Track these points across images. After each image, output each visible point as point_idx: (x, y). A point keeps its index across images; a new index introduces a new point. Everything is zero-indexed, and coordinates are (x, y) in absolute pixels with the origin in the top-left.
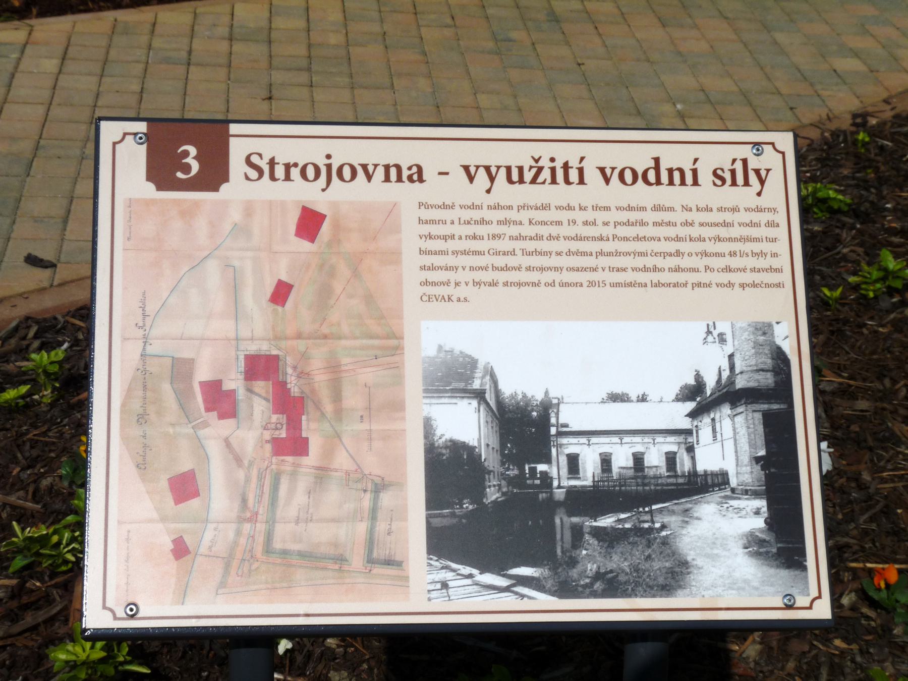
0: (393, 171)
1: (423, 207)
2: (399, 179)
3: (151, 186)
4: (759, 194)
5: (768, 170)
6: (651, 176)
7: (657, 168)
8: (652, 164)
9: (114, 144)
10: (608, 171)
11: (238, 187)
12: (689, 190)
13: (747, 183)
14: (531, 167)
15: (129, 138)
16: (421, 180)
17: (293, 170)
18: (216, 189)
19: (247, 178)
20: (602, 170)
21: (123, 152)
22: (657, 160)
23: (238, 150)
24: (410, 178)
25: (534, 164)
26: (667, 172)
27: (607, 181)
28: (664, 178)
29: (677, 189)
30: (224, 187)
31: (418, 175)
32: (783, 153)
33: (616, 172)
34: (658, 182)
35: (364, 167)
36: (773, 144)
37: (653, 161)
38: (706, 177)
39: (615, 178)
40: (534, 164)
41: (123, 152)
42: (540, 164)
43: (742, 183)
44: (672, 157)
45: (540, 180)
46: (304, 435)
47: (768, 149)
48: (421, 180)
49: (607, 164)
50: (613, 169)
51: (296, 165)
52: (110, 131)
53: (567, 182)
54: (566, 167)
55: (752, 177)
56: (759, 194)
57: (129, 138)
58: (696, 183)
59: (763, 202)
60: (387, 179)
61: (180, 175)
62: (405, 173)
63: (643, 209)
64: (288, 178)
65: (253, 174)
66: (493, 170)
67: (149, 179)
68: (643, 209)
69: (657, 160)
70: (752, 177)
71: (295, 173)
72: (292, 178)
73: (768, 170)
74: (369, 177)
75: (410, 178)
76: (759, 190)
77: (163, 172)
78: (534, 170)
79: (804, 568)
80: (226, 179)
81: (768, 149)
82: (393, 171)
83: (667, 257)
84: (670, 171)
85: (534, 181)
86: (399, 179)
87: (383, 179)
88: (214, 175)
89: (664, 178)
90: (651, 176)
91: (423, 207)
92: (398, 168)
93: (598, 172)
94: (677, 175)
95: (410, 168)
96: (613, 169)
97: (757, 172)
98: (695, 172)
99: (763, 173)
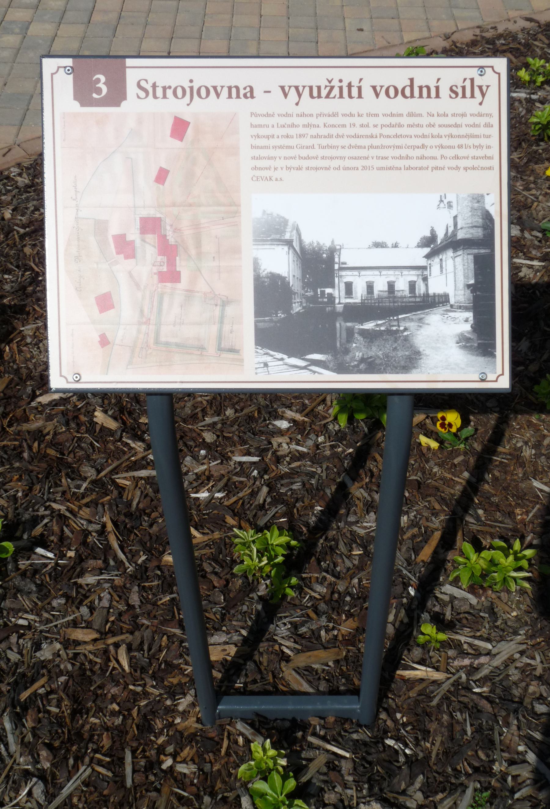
0: (234, 91)
2: (238, 97)
3: (77, 104)
4: (481, 104)
5: (488, 87)
6: (408, 92)
7: (412, 86)
8: (408, 83)
9: (52, 74)
10: (378, 89)
11: (132, 103)
12: (433, 101)
13: (473, 96)
14: (326, 86)
16: (252, 97)
17: (168, 90)
18: (118, 105)
19: (138, 97)
20: (374, 88)
22: (412, 80)
24: (245, 96)
25: (328, 84)
27: (377, 95)
29: (425, 101)
30: (124, 103)
31: (251, 94)
32: (499, 74)
34: (412, 96)
35: (215, 88)
36: (492, 67)
38: (445, 92)
39: (383, 94)
40: (328, 84)
42: (332, 84)
45: (332, 95)
47: (489, 71)
48: (252, 97)
49: (378, 84)
50: (382, 87)
51: (170, 87)
53: (350, 96)
54: (350, 86)
55: (477, 91)
56: (481, 104)
57: (61, 70)
58: (438, 96)
59: (483, 109)
60: (230, 96)
61: (95, 96)
62: (242, 92)
64: (165, 97)
65: (142, 94)
66: (301, 89)
67: (75, 98)
69: (412, 80)
71: (169, 93)
73: (488, 87)
75: (245, 96)
77: (84, 94)
78: (328, 89)
80: (125, 98)
81: (489, 71)
82: (234, 91)
84: (421, 88)
85: (327, 96)
88: (117, 96)
90: (408, 92)
92: (237, 88)
94: (425, 91)
95: (245, 89)
96: (382, 87)
97: (480, 88)
98: (437, 88)
99: (484, 89)
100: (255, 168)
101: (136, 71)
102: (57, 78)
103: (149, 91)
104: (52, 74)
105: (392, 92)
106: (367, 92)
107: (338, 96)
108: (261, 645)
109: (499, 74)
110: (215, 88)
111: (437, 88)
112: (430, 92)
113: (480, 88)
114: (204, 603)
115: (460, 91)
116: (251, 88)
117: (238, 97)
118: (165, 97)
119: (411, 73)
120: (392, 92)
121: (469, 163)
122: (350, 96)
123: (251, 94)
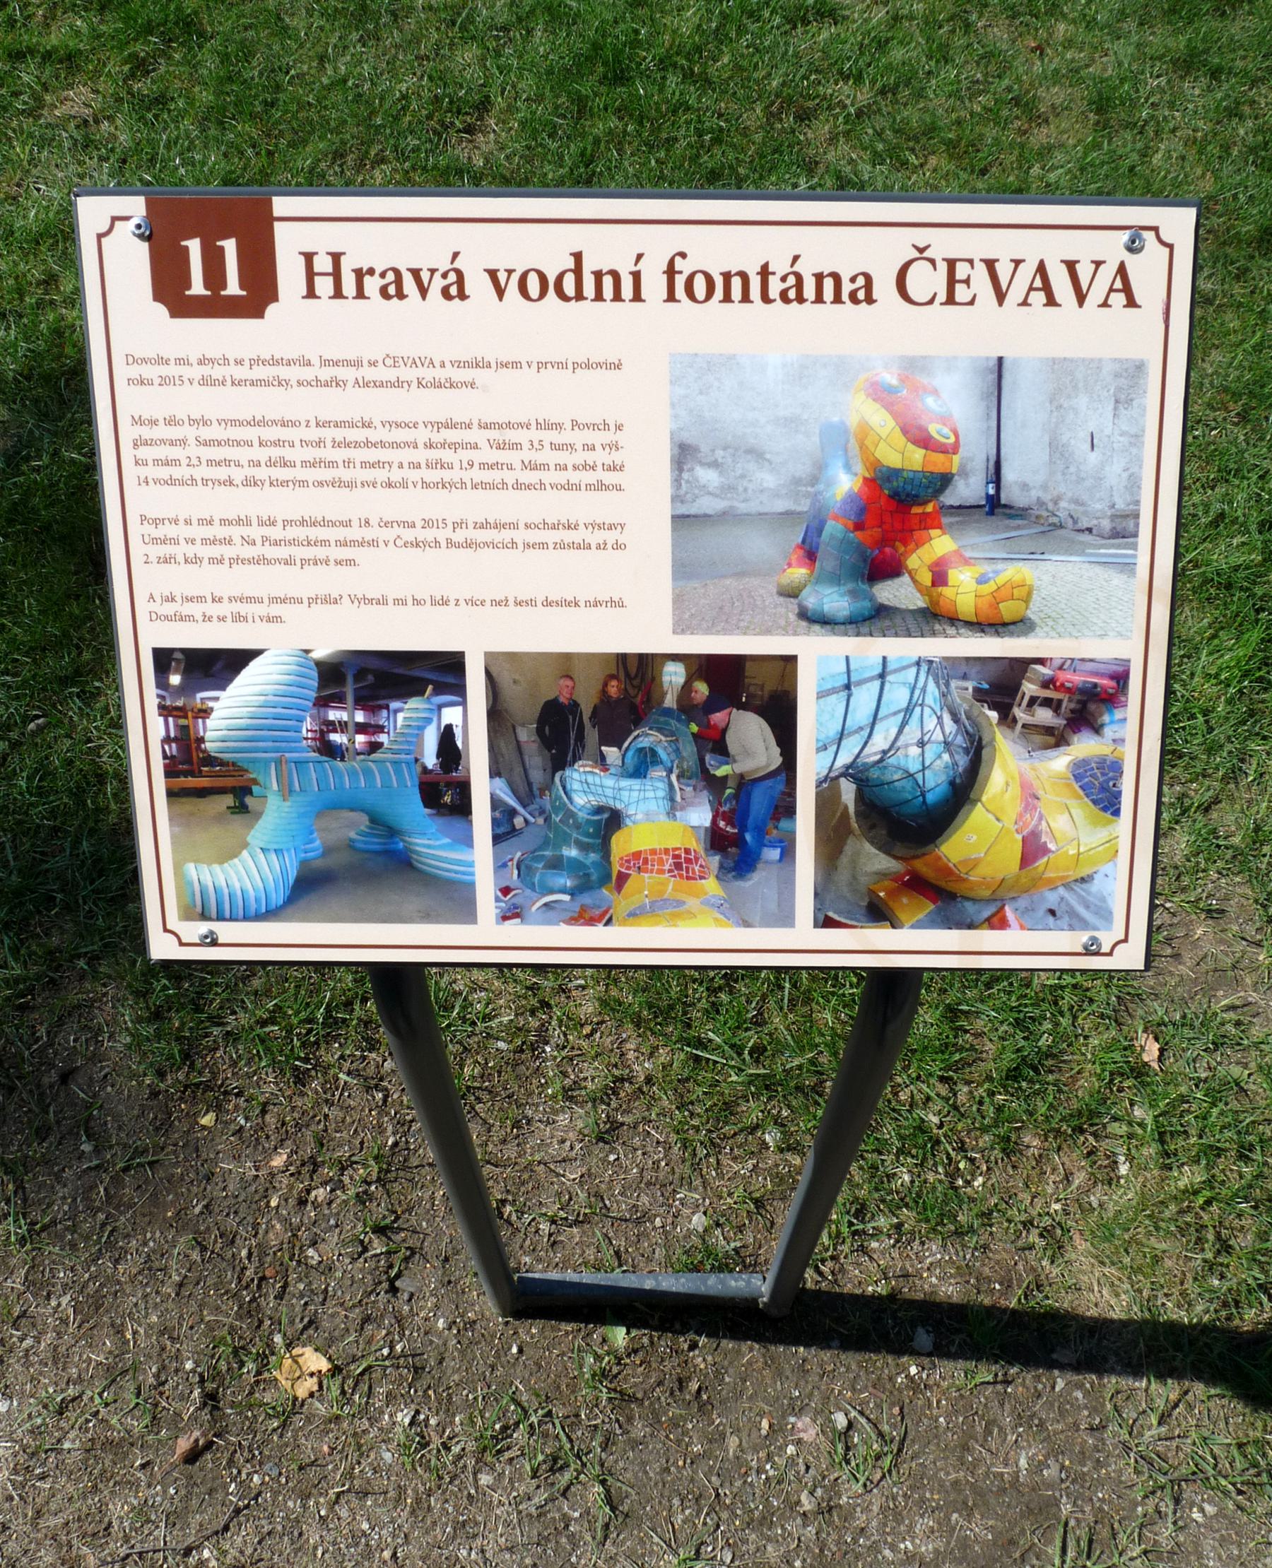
2: (838, 299)
6: (569, 286)
8: (571, 264)
10: (502, 277)
11: (293, 318)
17: (367, 279)
20: (493, 274)
21: (111, 235)
22: (578, 257)
23: (289, 244)
26: (593, 277)
27: (500, 292)
28: (349, 286)
29: (608, 306)
30: (271, 310)
33: (515, 278)
34: (579, 296)
35: (416, 273)
36: (1155, 229)
37: (572, 259)
39: (512, 289)
41: (111, 235)
43: (832, 298)
44: (608, 249)
46: (249, 839)
47: (1149, 236)
48: (462, 296)
49: (501, 265)
50: (510, 272)
51: (371, 272)
52: (92, 212)
53: (766, 298)
54: (765, 272)
58: (637, 297)
60: (338, 294)
62: (847, 288)
64: (360, 294)
67: (158, 296)
69: (578, 257)
72: (366, 294)
74: (423, 291)
77: (170, 289)
79: (1117, 813)
80: (274, 298)
83: (443, 430)
84: (598, 275)
86: (838, 299)
87: (304, 293)
88: (259, 294)
89: (349, 286)
90: (569, 286)
92: (836, 278)
94: (608, 282)
95: (853, 280)
96: (510, 272)
98: (636, 276)
101: (306, 226)
103: (334, 278)
105: (533, 285)
106: (478, 285)
107: (942, 296)
108: (1202, 1386)
110: (416, 273)
111: (636, 276)
112: (616, 287)
114: (619, 1336)
116: (868, 278)
118: (360, 294)
119: (576, 237)
120: (533, 285)
122: (766, 298)
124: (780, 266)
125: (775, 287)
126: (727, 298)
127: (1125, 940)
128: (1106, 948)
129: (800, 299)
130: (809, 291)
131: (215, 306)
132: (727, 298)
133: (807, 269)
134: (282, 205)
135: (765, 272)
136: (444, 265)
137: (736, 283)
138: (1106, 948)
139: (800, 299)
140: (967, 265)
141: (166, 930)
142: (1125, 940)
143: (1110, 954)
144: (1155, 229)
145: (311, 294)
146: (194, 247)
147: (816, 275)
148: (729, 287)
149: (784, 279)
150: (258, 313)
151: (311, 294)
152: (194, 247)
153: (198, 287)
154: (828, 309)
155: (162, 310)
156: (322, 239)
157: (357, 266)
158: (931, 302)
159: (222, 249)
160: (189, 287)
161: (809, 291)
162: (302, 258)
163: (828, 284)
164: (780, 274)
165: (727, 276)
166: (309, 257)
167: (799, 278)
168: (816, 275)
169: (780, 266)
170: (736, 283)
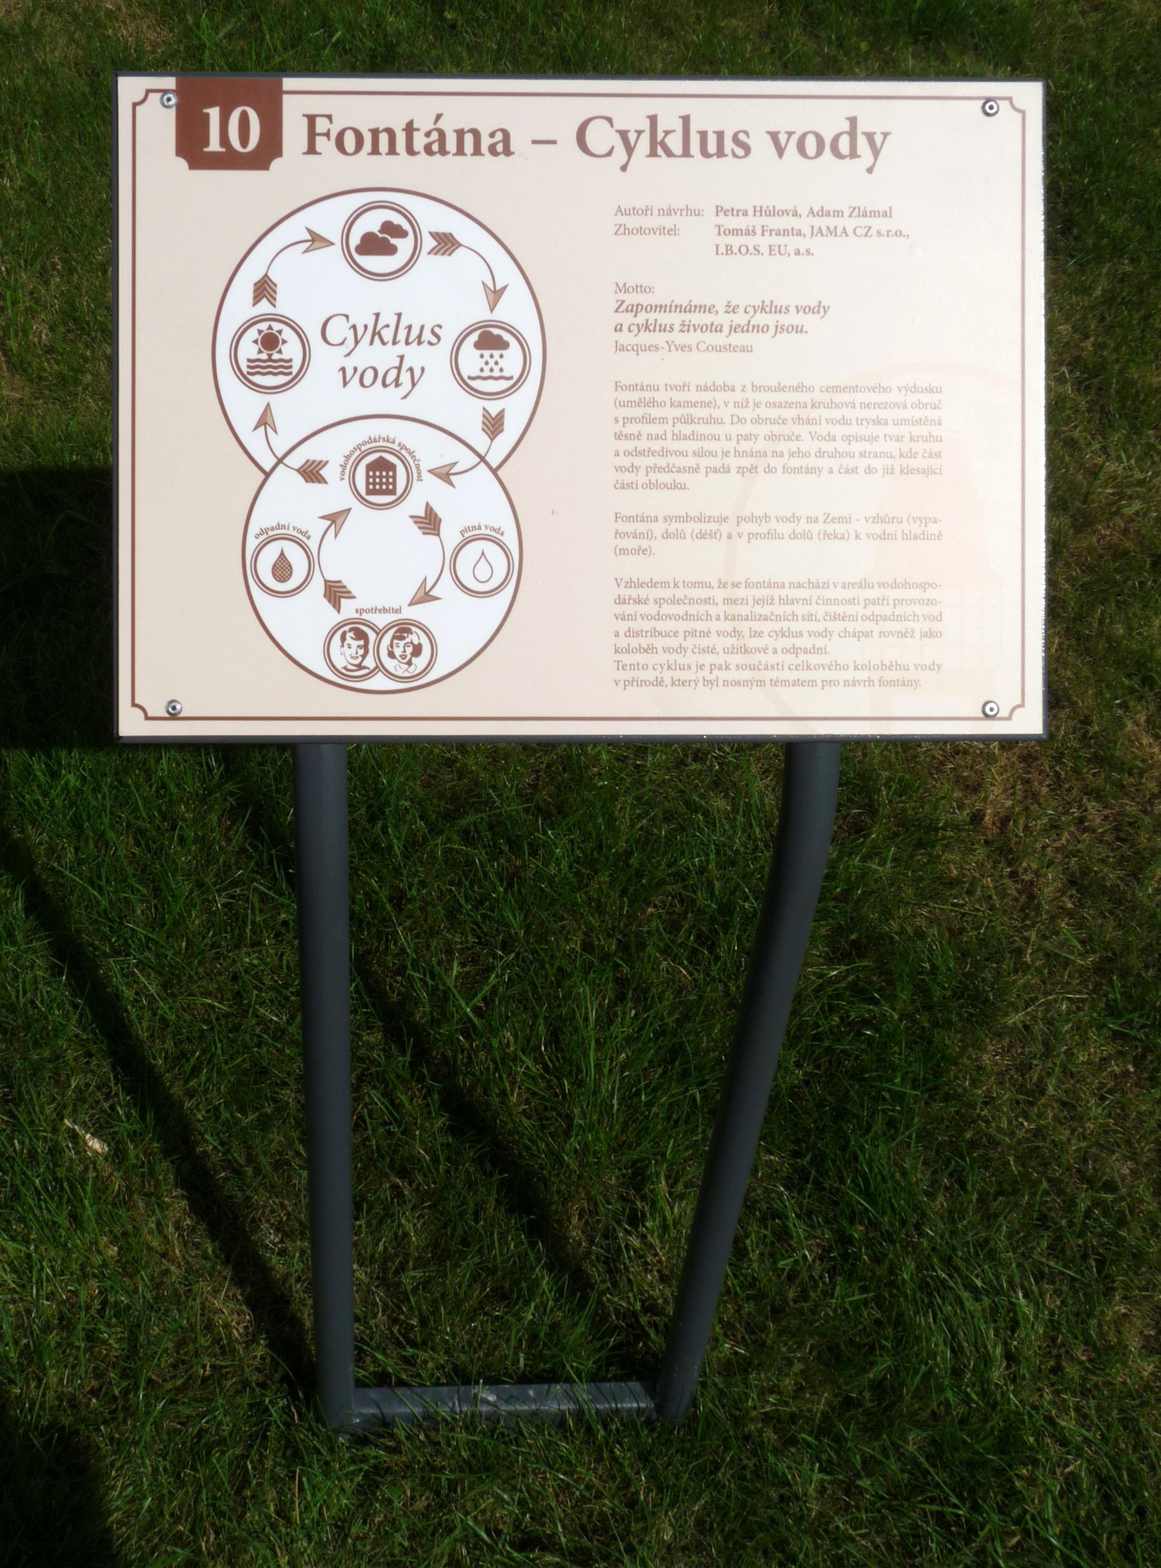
1: (721, 214)
2: (477, 151)
4: (870, 170)
5: (886, 135)
6: (844, 145)
8: (846, 126)
10: (783, 138)
15: (154, 98)
16: (507, 152)
20: (774, 136)
22: (853, 121)
24: (428, 149)
27: (780, 151)
29: (384, 160)
31: (504, 145)
32: (134, 705)
36: (1010, 99)
37: (318, 149)
39: (791, 149)
47: (1004, 105)
48: (507, 152)
49: (782, 128)
50: (790, 134)
52: (129, 88)
53: (411, 151)
54: (410, 129)
55: (862, 142)
62: (486, 142)
63: (838, 213)
66: (632, 137)
68: (838, 213)
69: (853, 121)
70: (862, 142)
73: (886, 135)
75: (493, 150)
76: (623, 162)
77: (192, 147)
81: (1004, 105)
87: (305, 149)
88: (268, 151)
90: (844, 145)
91: (721, 214)
92: (476, 133)
93: (768, 138)
95: (492, 135)
96: (790, 134)
97: (870, 136)
99: (878, 139)
100: (935, 407)
101: (304, 97)
102: (145, 109)
104: (135, 105)
105: (811, 145)
109: (134, 705)
113: (870, 136)
115: (729, 145)
116: (506, 135)
117: (477, 151)
120: (811, 145)
121: (859, 397)
122: (411, 151)
123: (504, 145)
124: (424, 123)
125: (419, 141)
126: (375, 151)
127: (147, 718)
128: (1004, 713)
129: (443, 151)
130: (451, 144)
131: (229, 160)
132: (375, 151)
133: (449, 126)
134: (289, 83)
135: (410, 129)
136: (430, 125)
137: (384, 139)
138: (1004, 713)
139: (443, 151)
140: (326, 120)
141: (1023, 112)
142: (1022, 705)
143: (1009, 718)
144: (1010, 99)
145: (312, 150)
146: (214, 113)
147: (456, 131)
148: (379, 141)
149: (428, 135)
150: (265, 166)
151: (312, 150)
152: (214, 113)
153: (214, 145)
154: (469, 160)
155: (182, 163)
156: (315, 105)
157: (373, 127)
158: (609, 154)
159: (208, 115)
160: (207, 145)
161: (451, 144)
162: (305, 120)
163: (469, 139)
164: (424, 130)
165: (375, 133)
166: (311, 119)
167: (442, 134)
168: (456, 131)
169: (424, 123)
170: (384, 139)
